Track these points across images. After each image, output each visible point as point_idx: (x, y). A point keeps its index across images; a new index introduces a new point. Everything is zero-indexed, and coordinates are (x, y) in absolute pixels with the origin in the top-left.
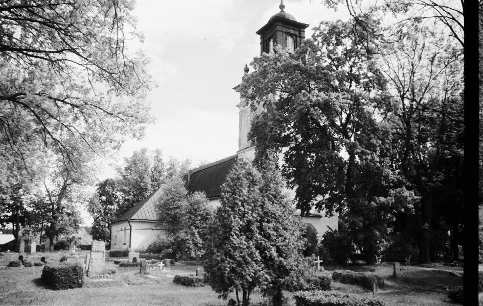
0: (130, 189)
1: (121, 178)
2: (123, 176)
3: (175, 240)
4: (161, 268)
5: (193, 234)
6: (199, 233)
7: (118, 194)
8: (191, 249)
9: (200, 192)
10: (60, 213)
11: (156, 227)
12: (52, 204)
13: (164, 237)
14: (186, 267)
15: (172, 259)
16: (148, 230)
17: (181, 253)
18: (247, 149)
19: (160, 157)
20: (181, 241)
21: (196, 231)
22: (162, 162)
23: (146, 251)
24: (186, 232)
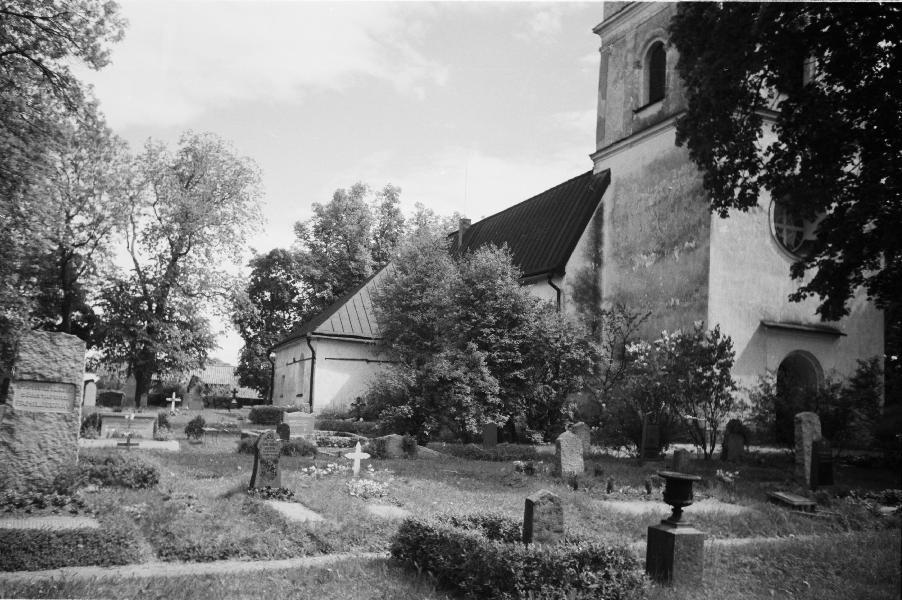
0: (326, 273)
1: (307, 250)
2: (312, 246)
3: (420, 379)
4: (356, 468)
5: (473, 366)
6: (490, 362)
7: (299, 285)
8: (466, 409)
9: (494, 247)
10: (165, 321)
11: (377, 355)
12: (146, 297)
13: (394, 376)
14: (452, 468)
15: (407, 436)
16: (356, 362)
17: (438, 420)
18: (624, 143)
19: (395, 206)
20: (438, 384)
21: (482, 356)
22: (399, 216)
23: (350, 412)
24: (453, 359)
